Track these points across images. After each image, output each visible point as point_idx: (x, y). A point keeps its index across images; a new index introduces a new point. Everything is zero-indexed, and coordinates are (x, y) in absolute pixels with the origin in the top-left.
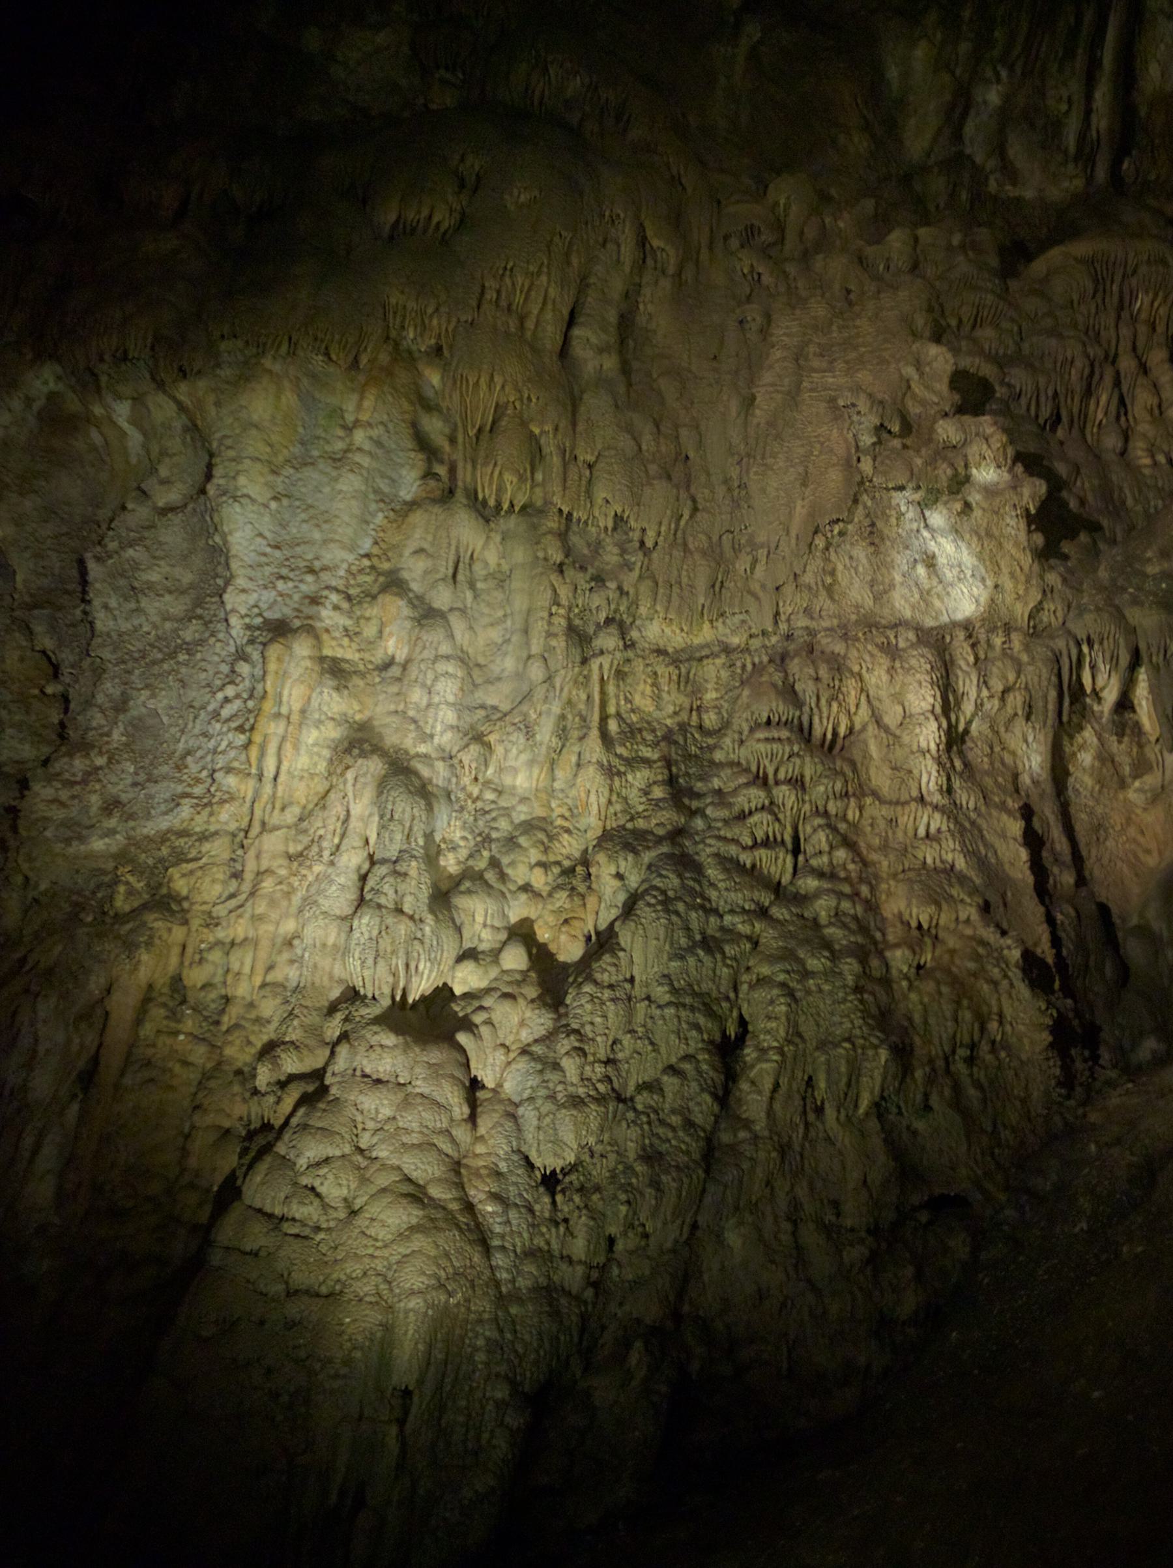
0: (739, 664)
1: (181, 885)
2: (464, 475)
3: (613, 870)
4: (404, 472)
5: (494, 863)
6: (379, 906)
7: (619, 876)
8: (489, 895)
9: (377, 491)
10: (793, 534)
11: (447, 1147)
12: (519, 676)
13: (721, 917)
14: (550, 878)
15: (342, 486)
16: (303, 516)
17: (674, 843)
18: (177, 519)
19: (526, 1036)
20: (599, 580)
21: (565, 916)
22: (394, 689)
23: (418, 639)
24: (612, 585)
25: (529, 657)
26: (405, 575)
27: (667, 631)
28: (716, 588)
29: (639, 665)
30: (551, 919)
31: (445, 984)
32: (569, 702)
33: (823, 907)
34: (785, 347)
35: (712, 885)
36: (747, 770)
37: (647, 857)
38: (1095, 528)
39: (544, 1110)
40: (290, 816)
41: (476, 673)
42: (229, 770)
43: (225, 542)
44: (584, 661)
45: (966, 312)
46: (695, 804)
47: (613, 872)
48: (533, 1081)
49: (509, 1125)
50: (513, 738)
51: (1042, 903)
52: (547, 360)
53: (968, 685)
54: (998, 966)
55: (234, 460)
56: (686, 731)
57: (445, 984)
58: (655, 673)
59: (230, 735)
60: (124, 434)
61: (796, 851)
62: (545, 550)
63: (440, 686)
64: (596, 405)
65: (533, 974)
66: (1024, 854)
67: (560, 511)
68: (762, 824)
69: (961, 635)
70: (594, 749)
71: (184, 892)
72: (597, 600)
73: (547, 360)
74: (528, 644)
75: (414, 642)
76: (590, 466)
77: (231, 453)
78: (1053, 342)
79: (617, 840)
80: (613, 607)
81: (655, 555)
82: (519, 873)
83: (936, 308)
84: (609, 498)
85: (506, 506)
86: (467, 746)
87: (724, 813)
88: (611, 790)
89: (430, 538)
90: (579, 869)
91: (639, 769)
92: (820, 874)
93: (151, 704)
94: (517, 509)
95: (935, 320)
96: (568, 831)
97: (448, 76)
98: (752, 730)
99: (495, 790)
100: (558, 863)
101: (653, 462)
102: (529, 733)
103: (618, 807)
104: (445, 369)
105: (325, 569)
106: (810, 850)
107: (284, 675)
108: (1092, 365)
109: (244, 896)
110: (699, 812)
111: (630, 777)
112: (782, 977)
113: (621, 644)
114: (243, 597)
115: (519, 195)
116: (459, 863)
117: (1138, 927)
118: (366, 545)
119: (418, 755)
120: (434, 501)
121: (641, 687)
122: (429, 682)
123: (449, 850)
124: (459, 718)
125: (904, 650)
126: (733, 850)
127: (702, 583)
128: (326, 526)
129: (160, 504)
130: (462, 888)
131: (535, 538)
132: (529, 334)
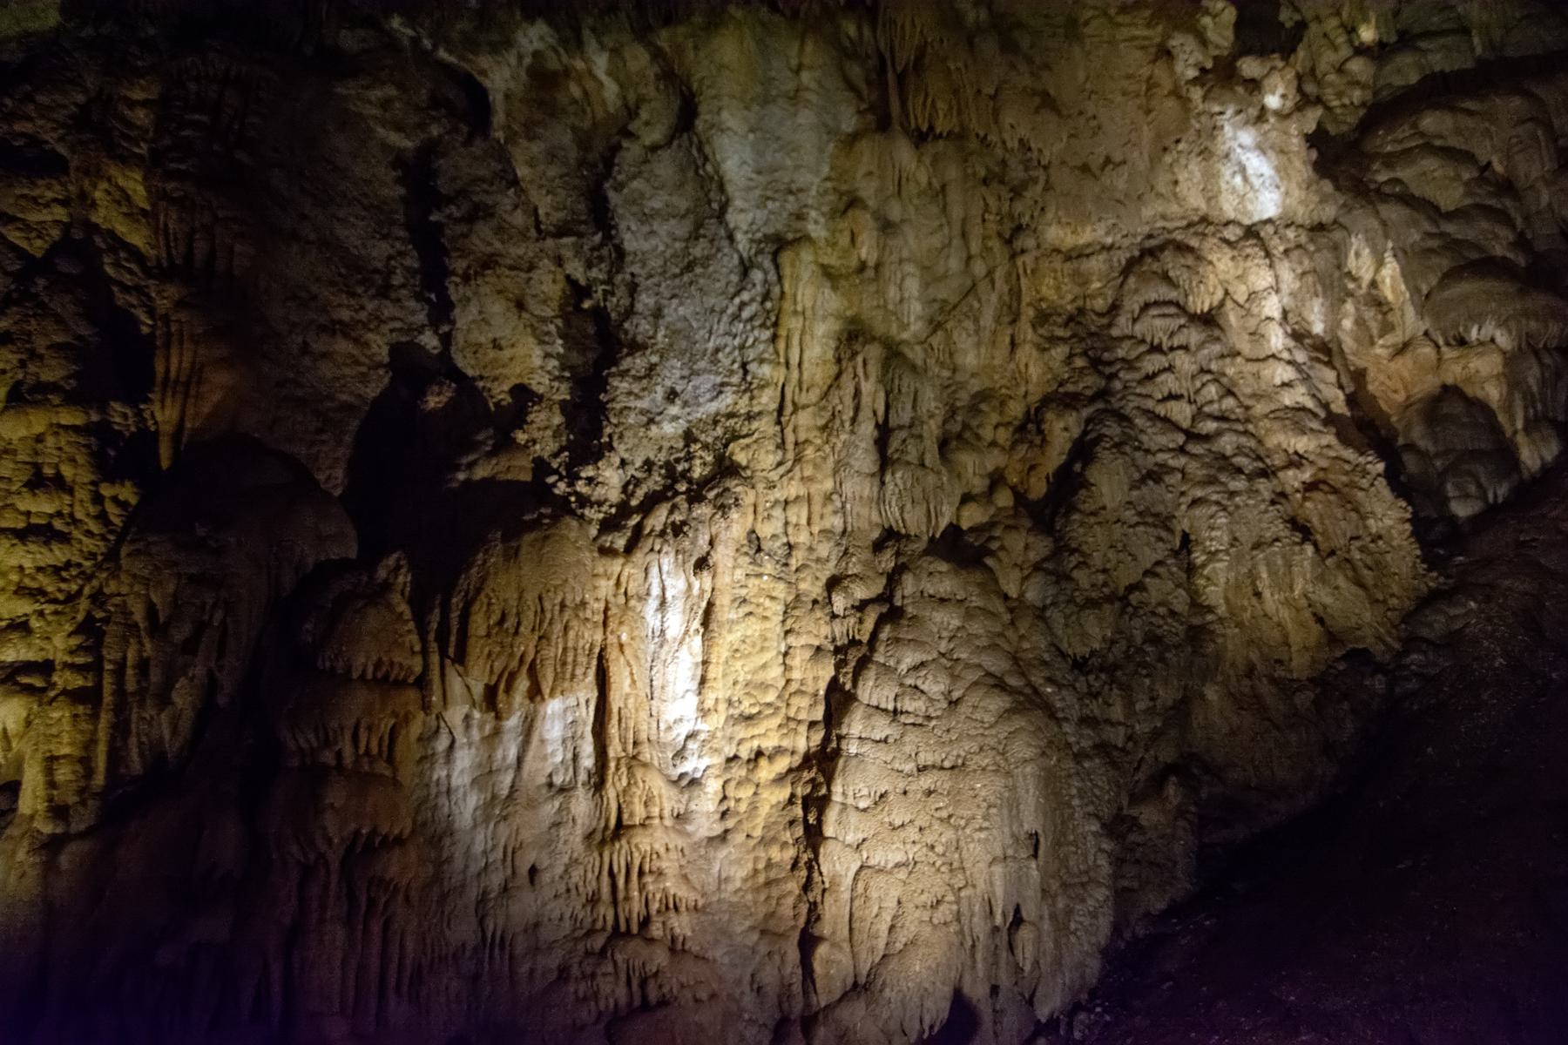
1: (741, 458)
3: (1062, 425)
6: (908, 463)
11: (1006, 647)
15: (801, 120)
16: (775, 146)
18: (665, 155)
19: (1033, 556)
22: (873, 288)
30: (1019, 466)
33: (1227, 444)
39: (1068, 611)
40: (814, 396)
42: (762, 361)
43: (717, 172)
48: (1052, 591)
49: (1041, 625)
55: (715, 97)
59: (756, 333)
60: (601, 84)
71: (744, 463)
74: (968, 248)
75: (882, 249)
77: (713, 92)
82: (987, 433)
87: (1137, 376)
93: (681, 311)
105: (801, 190)
107: (796, 279)
109: (790, 464)
112: (1215, 497)
114: (742, 216)
118: (826, 170)
126: (1150, 404)
128: (794, 154)
129: (647, 142)
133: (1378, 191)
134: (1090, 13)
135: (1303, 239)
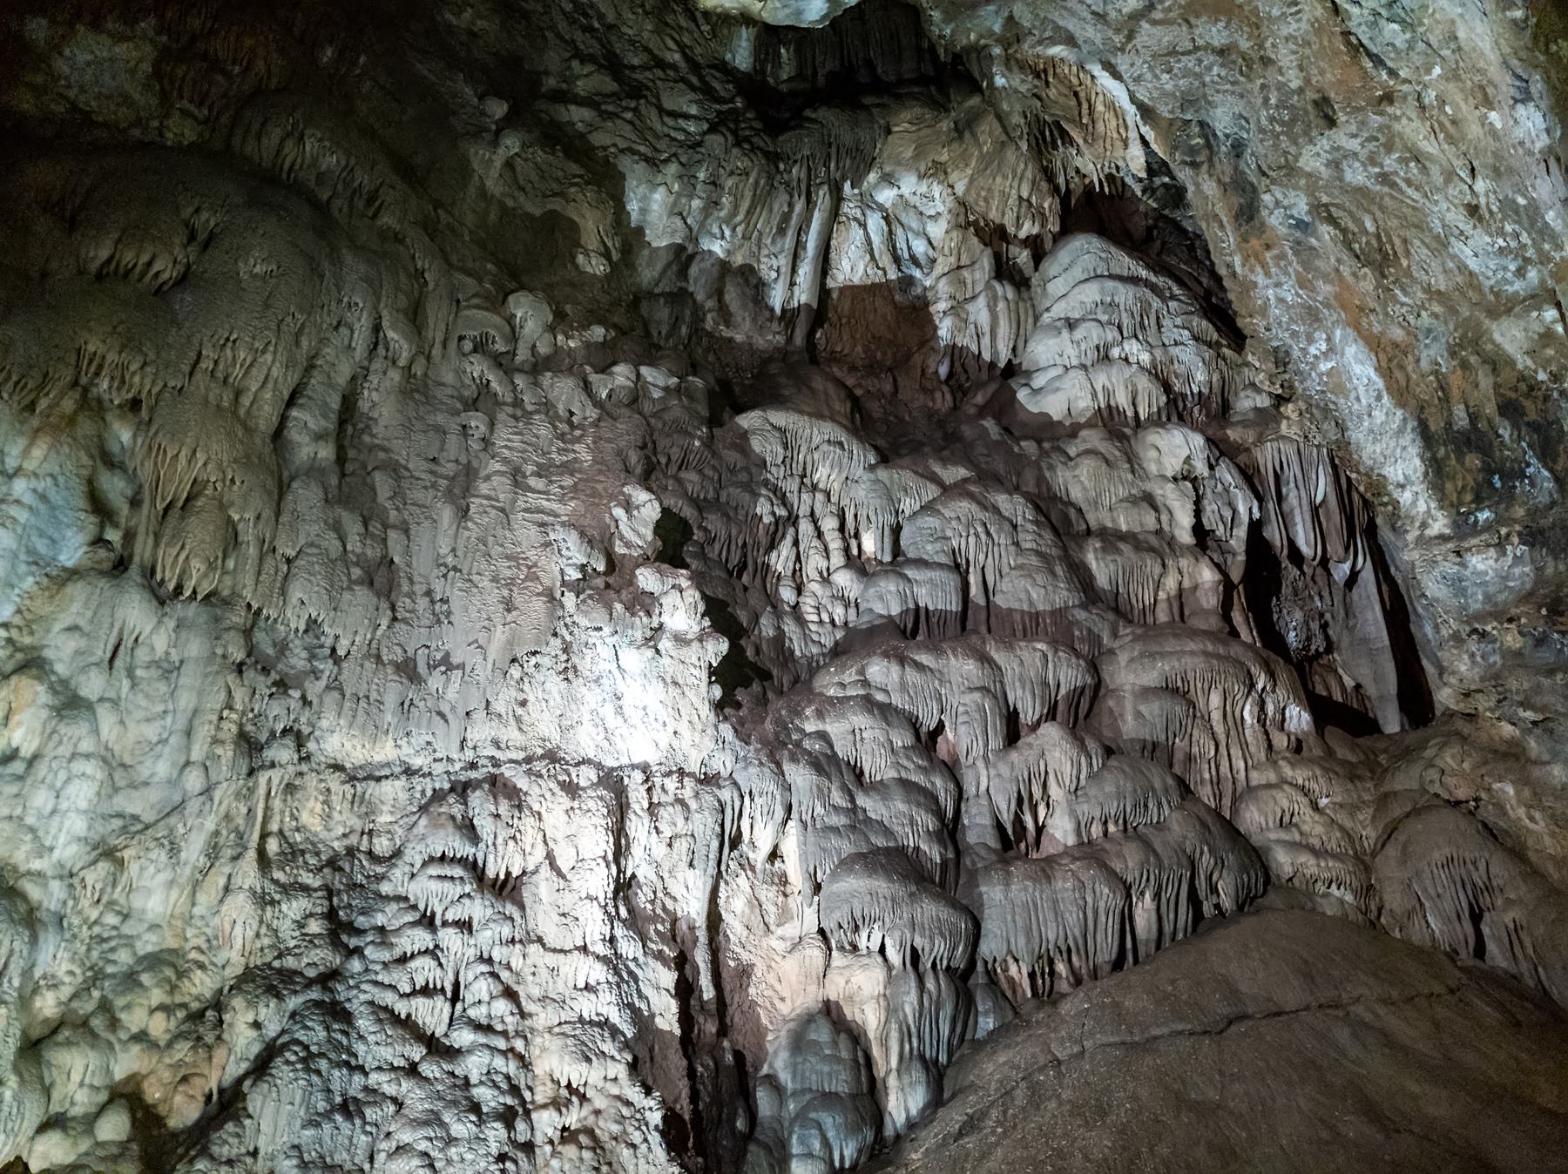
0: (419, 788)
2: (143, 549)
3: (250, 1018)
4: (69, 534)
5: (105, 1006)
7: (257, 1025)
8: (93, 1047)
9: (30, 551)
10: (490, 661)
12: (173, 783)
13: (366, 1074)
14: (173, 1023)
17: (326, 988)
20: (282, 685)
21: (183, 1072)
23: (54, 731)
24: (296, 694)
25: (188, 763)
26: (48, 654)
27: (348, 745)
28: (406, 707)
29: (311, 781)
30: (166, 1075)
31: (18, 1158)
32: (228, 817)
33: (474, 1066)
34: (505, 461)
35: (361, 1037)
36: (414, 907)
37: (293, 1002)
38: (766, 676)
41: (118, 775)
44: (251, 772)
45: (676, 453)
46: (353, 942)
47: (251, 1020)
50: (153, 855)
51: (686, 1055)
52: (258, 441)
53: (638, 827)
54: (639, 1128)
56: (353, 856)
57: (18, 1158)
58: (328, 790)
61: (455, 998)
62: (225, 647)
63: (72, 789)
64: (305, 497)
65: (134, 1146)
66: (673, 1006)
67: (249, 606)
68: (424, 971)
69: (638, 776)
70: (248, 874)
72: (276, 708)
73: (258, 441)
74: (188, 749)
76: (289, 561)
78: (747, 496)
79: (259, 981)
80: (292, 717)
81: (345, 665)
82: (134, 1020)
83: (648, 447)
84: (305, 600)
85: (187, 593)
86: (95, 862)
87: (386, 956)
88: (261, 922)
89: (89, 614)
90: (209, 1013)
91: (296, 898)
92: (478, 1027)
94: (199, 597)
95: (647, 457)
96: (202, 966)
97: (192, 108)
98: (425, 864)
99: (119, 913)
100: (184, 1006)
101: (357, 564)
102: (174, 850)
103: (266, 941)
104: (142, 427)
106: (469, 999)
108: (777, 523)
110: (358, 951)
111: (284, 907)
112: (423, 1146)
113: (296, 757)
115: (255, 265)
116: (60, 1004)
117: (767, 1076)
119: (29, 873)
120: (102, 573)
121: (311, 804)
122: (59, 784)
123: (49, 987)
124: (89, 828)
125: (583, 789)
126: (389, 998)
127: (391, 700)
130: (60, 1037)
131: (217, 630)
132: (242, 412)
133: (798, 744)
134: (498, 466)
135: (687, 793)
